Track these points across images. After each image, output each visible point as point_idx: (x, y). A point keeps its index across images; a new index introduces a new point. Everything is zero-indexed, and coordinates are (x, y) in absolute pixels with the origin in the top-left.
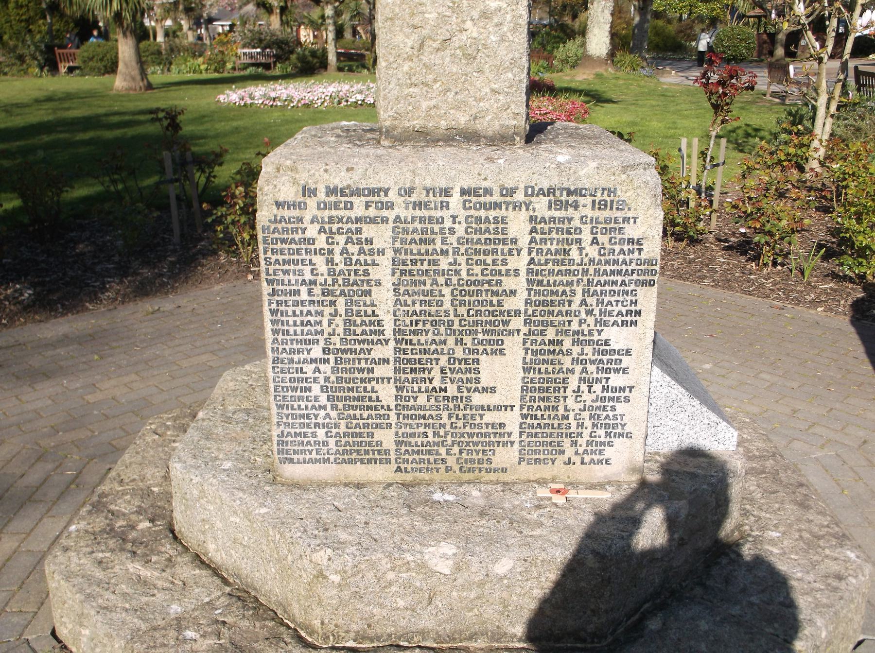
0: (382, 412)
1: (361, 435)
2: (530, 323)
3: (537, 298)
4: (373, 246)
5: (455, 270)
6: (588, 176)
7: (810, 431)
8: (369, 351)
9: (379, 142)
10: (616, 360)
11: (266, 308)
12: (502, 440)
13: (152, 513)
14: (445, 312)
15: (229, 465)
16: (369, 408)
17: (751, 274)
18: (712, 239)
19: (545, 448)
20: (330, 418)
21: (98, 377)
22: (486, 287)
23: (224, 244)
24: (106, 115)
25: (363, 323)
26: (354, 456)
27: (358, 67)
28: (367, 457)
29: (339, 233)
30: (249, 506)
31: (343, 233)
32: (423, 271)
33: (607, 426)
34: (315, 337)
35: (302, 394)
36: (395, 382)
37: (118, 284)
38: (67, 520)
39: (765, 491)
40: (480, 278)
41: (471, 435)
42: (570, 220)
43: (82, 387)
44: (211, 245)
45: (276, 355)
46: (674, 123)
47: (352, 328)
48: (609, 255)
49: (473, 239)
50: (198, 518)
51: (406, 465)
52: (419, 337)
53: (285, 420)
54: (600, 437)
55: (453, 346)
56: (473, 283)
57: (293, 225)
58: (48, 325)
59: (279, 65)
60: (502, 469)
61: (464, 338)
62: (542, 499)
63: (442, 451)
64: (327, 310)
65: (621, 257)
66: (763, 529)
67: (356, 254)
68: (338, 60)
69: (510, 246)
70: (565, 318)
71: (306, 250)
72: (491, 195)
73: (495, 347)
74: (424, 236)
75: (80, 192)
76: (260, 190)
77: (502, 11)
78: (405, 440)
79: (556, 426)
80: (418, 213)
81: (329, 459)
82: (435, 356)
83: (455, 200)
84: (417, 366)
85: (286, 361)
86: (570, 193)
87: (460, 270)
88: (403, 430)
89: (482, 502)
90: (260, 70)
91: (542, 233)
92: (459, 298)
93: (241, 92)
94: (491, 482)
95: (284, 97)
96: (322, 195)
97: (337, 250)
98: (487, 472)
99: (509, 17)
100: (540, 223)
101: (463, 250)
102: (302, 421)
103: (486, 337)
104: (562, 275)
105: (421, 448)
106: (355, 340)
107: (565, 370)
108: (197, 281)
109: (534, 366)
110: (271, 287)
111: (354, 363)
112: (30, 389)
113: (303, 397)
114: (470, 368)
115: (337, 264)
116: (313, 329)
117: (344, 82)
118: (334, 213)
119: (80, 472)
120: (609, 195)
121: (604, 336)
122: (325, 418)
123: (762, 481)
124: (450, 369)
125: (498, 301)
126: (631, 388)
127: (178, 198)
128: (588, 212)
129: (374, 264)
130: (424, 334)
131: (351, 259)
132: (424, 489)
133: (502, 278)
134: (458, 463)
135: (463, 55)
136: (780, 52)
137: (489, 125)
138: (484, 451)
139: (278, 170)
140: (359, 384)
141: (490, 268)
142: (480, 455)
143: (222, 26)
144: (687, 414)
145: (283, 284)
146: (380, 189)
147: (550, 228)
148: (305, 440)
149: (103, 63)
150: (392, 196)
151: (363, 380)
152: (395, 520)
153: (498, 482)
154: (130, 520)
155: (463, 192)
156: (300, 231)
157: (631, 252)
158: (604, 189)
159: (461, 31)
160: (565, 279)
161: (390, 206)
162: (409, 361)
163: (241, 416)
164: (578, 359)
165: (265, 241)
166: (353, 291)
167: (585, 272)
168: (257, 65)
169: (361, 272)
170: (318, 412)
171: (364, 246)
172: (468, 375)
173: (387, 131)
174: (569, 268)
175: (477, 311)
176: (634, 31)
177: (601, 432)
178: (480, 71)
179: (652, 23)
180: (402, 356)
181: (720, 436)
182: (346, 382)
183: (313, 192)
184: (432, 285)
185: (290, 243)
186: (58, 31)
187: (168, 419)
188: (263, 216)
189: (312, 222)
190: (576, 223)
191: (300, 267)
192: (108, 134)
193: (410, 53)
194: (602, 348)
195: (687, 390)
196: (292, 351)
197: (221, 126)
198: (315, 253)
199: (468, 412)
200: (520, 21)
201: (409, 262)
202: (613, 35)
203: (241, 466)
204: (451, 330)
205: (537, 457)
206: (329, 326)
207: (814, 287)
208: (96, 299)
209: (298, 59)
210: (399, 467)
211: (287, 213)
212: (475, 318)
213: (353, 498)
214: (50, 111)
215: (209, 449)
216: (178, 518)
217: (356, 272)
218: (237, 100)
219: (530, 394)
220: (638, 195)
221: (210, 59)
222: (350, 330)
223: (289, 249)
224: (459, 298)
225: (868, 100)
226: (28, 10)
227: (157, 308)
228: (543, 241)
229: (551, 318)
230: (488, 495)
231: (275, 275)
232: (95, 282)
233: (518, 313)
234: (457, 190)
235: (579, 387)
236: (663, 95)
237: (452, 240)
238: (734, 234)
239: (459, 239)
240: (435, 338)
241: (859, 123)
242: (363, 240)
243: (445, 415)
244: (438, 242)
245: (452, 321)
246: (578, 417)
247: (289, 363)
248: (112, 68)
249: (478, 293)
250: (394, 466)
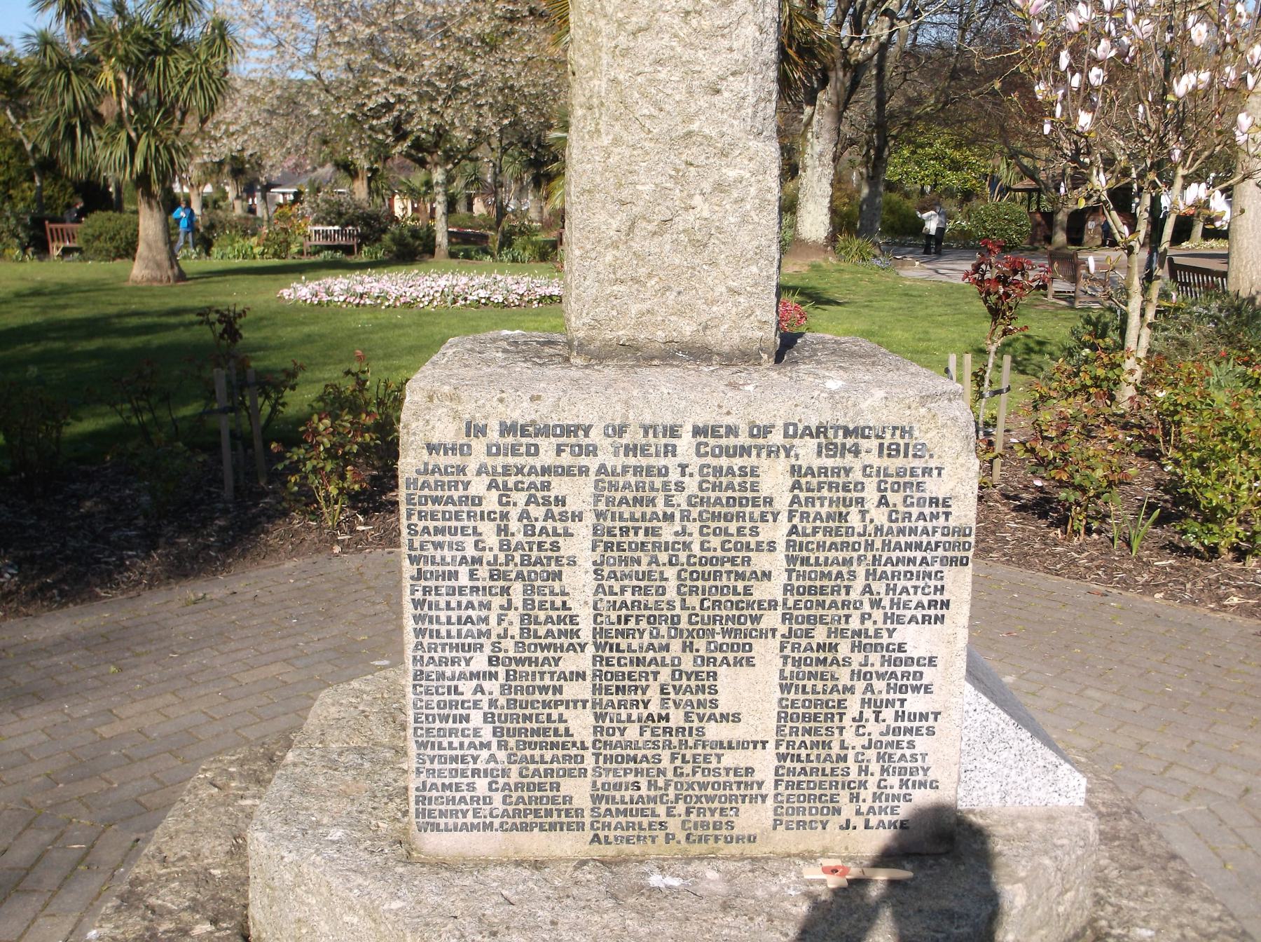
0: (574, 752)
1: (541, 787)
2: (790, 619)
3: (801, 583)
4: (566, 508)
5: (684, 543)
6: (873, 410)
7: (1167, 775)
8: (557, 661)
9: (567, 360)
10: (915, 673)
11: (407, 598)
12: (749, 792)
13: (213, 909)
14: (668, 603)
15: (339, 834)
16: (554, 746)
17: (1056, 545)
18: (997, 496)
19: (812, 804)
20: (496, 762)
21: (115, 699)
22: (728, 566)
23: (298, 501)
24: (119, 316)
25: (549, 619)
26: (530, 818)
27: (477, 251)
28: (549, 819)
29: (517, 489)
30: (374, 897)
31: (522, 489)
32: (637, 544)
33: (902, 771)
34: (478, 641)
35: (455, 726)
36: (593, 707)
37: (143, 560)
38: (75, 920)
39: (1122, 866)
40: (719, 553)
41: (703, 786)
42: (848, 471)
43: (91, 715)
44: (279, 503)
45: (419, 667)
46: (927, 333)
47: (532, 627)
48: (903, 521)
49: (709, 498)
50: (291, 917)
51: (606, 832)
52: (630, 640)
53: (428, 765)
54: (892, 787)
55: (679, 654)
56: (710, 561)
57: (451, 478)
58: (39, 621)
59: (365, 249)
60: (749, 837)
61: (696, 641)
62: (811, 882)
63: (661, 810)
64: (498, 601)
65: (921, 524)
66: (1128, 924)
67: (541, 519)
68: (450, 242)
69: (763, 509)
70: (841, 612)
71: (468, 513)
72: (736, 436)
73: (740, 655)
74: (640, 494)
75: (88, 425)
76: (405, 427)
77: (744, 183)
78: (606, 793)
79: (828, 771)
80: (632, 461)
81: (492, 823)
82: (653, 668)
83: (686, 443)
84: (627, 683)
85: (434, 677)
86: (847, 433)
87: (691, 543)
88: (603, 779)
89: (721, 888)
90: (338, 255)
91: (808, 490)
92: (689, 583)
93: (313, 285)
94: (732, 858)
95: (376, 293)
96: (494, 435)
97: (514, 513)
98: (727, 842)
99: (753, 191)
100: (806, 475)
101: (695, 513)
102: (454, 766)
103: (727, 640)
104: (837, 550)
105: (629, 806)
106: (536, 645)
107: (840, 688)
108: (259, 555)
109: (795, 682)
110: (415, 567)
111: (534, 679)
112: (14, 718)
113: (457, 730)
114: (703, 686)
115: (513, 534)
116: (475, 629)
117: (460, 272)
118: (511, 460)
119: (93, 846)
120: (902, 437)
121: (897, 638)
122: (488, 762)
123: (1116, 852)
124: (674, 687)
125: (745, 587)
126: (936, 715)
127: (233, 435)
128: (873, 460)
129: (567, 534)
130: (637, 635)
131: (534, 526)
132: (634, 869)
133: (750, 554)
134: (683, 828)
135: (690, 241)
136: (1060, 237)
137: (725, 336)
138: (722, 809)
139: (431, 398)
140: (541, 710)
141: (733, 539)
142: (717, 815)
143: (284, 194)
144: (1013, 751)
145: (433, 563)
146: (578, 427)
147: (819, 483)
148: (458, 795)
149: (115, 244)
150: (596, 436)
151: (546, 704)
152: (596, 918)
153: (742, 858)
154: (181, 921)
155: (697, 431)
156: (460, 486)
157: (935, 516)
158: (895, 428)
159: (686, 209)
160: (841, 555)
161: (592, 451)
162: (614, 676)
163: (352, 758)
164: (860, 671)
165: (409, 500)
166: (536, 573)
167: (869, 546)
168: (335, 248)
169: (547, 546)
170: (478, 752)
171: (553, 507)
172: (701, 697)
173: (581, 344)
174: (846, 539)
175: (714, 602)
176: (861, 207)
177: (894, 780)
178: (713, 263)
179: (885, 197)
180: (605, 669)
181: (1061, 785)
182: (521, 707)
183: (482, 431)
184: (649, 564)
185: (446, 504)
186: (50, 197)
187: (231, 763)
188: (408, 465)
189: (479, 473)
190: (857, 475)
191: (459, 538)
192: (125, 343)
194: (894, 655)
195: (1012, 716)
196: (444, 661)
197: (288, 333)
198: (482, 518)
199: (700, 750)
200: (769, 196)
201: (617, 532)
202: (833, 211)
203: (358, 835)
204: (676, 629)
205: (801, 818)
206: (499, 624)
207: (1148, 564)
208: (110, 581)
209: (393, 240)
210: (596, 836)
211: (442, 460)
212: (711, 613)
213: (531, 884)
214: (37, 310)
215: (307, 809)
216: (257, 917)
217: (540, 545)
218: (309, 296)
219: (790, 724)
220: (944, 436)
221: (267, 240)
222: (529, 630)
223: (444, 513)
224: (689, 583)
225: (1194, 304)
226: (8, 168)
227: (201, 595)
228: (810, 501)
229: (821, 612)
230: (730, 878)
231: (422, 549)
232: (110, 556)
233: (773, 605)
234: (688, 428)
235: (861, 713)
236: (907, 295)
237: (680, 499)
238: (1026, 488)
239: (690, 497)
240: (653, 641)
241: (1186, 336)
242: (552, 499)
243: (666, 755)
244: (660, 501)
245: (678, 616)
246: (860, 758)
247: (438, 680)
248: (126, 251)
249: (717, 575)
250: (589, 834)
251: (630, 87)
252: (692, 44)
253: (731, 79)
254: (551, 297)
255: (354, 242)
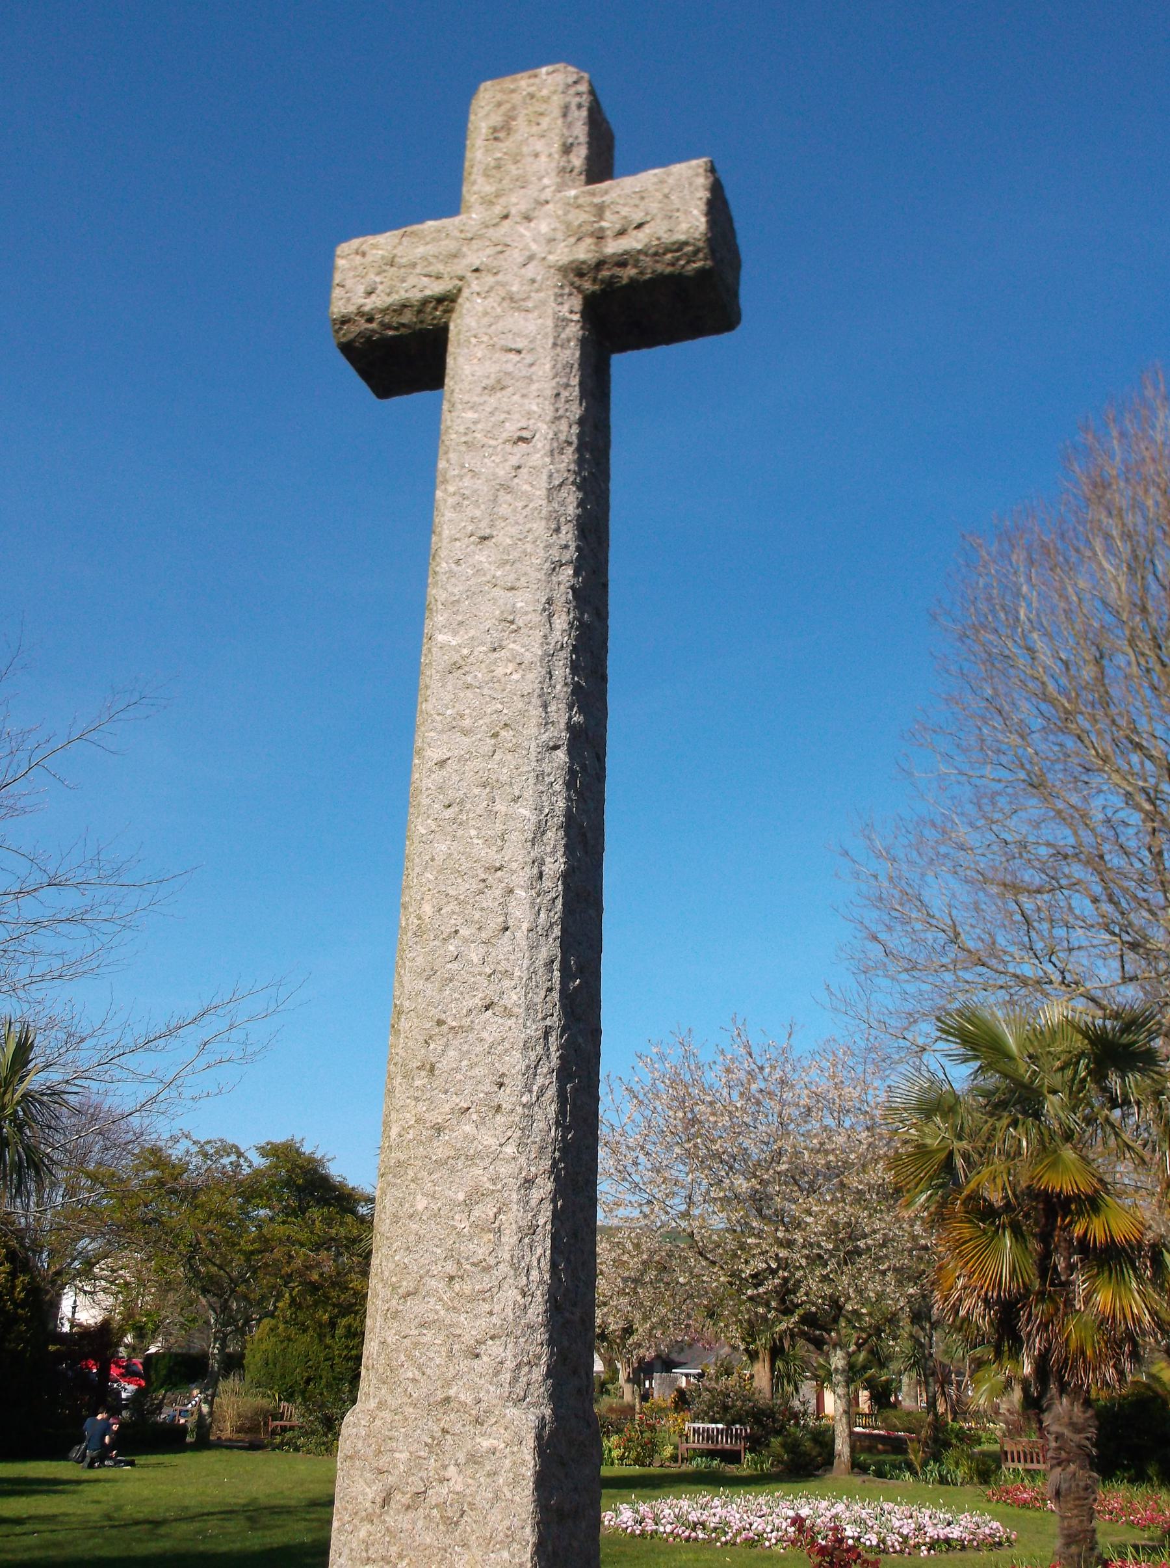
95: (712, 1523)
135: (441, 1517)
143: (687, 1375)
193: (370, 1510)
251: (397, 1350)
252: (454, 1308)
253: (490, 1342)
254: (947, 1540)
255: (740, 1446)
